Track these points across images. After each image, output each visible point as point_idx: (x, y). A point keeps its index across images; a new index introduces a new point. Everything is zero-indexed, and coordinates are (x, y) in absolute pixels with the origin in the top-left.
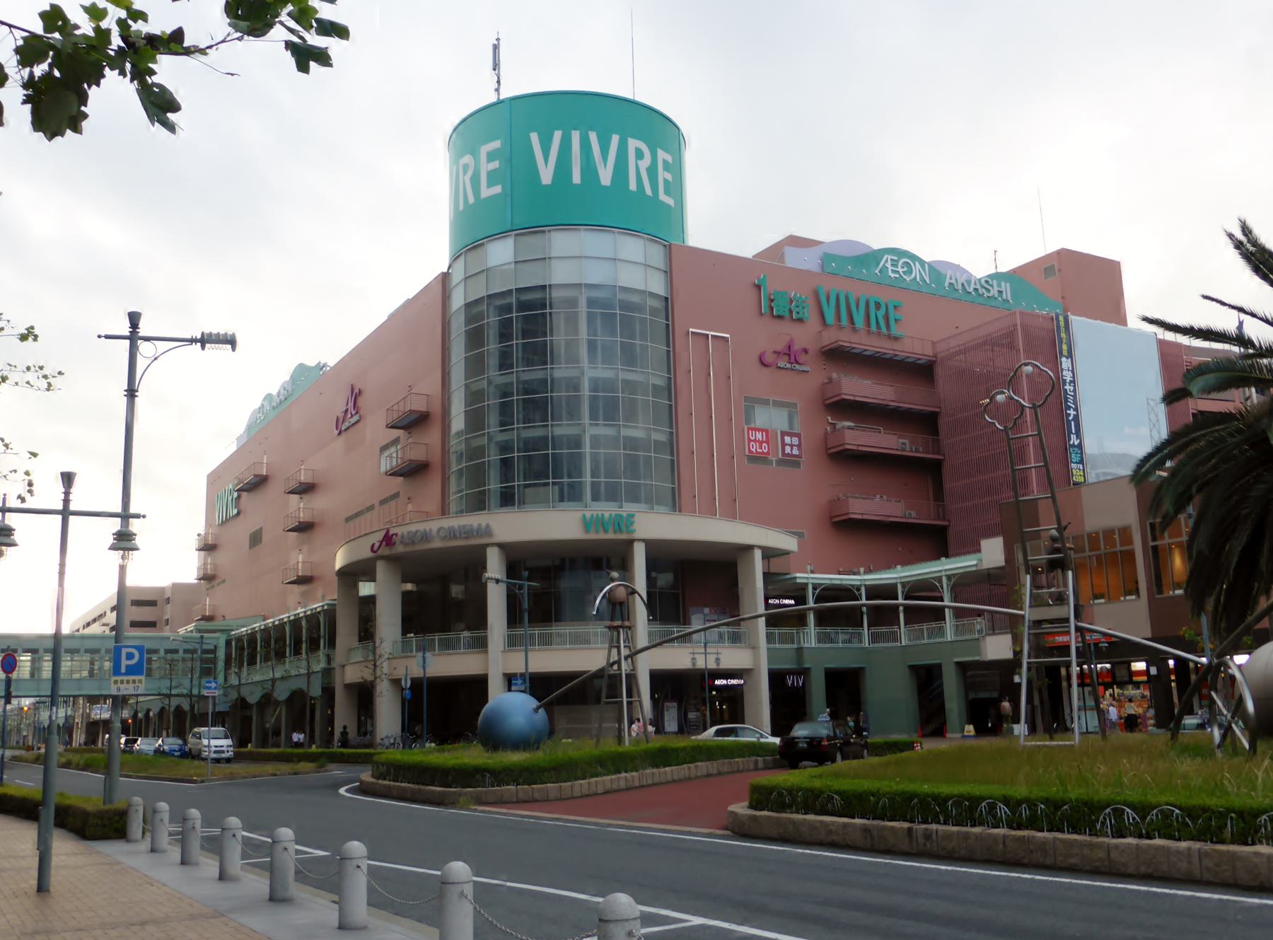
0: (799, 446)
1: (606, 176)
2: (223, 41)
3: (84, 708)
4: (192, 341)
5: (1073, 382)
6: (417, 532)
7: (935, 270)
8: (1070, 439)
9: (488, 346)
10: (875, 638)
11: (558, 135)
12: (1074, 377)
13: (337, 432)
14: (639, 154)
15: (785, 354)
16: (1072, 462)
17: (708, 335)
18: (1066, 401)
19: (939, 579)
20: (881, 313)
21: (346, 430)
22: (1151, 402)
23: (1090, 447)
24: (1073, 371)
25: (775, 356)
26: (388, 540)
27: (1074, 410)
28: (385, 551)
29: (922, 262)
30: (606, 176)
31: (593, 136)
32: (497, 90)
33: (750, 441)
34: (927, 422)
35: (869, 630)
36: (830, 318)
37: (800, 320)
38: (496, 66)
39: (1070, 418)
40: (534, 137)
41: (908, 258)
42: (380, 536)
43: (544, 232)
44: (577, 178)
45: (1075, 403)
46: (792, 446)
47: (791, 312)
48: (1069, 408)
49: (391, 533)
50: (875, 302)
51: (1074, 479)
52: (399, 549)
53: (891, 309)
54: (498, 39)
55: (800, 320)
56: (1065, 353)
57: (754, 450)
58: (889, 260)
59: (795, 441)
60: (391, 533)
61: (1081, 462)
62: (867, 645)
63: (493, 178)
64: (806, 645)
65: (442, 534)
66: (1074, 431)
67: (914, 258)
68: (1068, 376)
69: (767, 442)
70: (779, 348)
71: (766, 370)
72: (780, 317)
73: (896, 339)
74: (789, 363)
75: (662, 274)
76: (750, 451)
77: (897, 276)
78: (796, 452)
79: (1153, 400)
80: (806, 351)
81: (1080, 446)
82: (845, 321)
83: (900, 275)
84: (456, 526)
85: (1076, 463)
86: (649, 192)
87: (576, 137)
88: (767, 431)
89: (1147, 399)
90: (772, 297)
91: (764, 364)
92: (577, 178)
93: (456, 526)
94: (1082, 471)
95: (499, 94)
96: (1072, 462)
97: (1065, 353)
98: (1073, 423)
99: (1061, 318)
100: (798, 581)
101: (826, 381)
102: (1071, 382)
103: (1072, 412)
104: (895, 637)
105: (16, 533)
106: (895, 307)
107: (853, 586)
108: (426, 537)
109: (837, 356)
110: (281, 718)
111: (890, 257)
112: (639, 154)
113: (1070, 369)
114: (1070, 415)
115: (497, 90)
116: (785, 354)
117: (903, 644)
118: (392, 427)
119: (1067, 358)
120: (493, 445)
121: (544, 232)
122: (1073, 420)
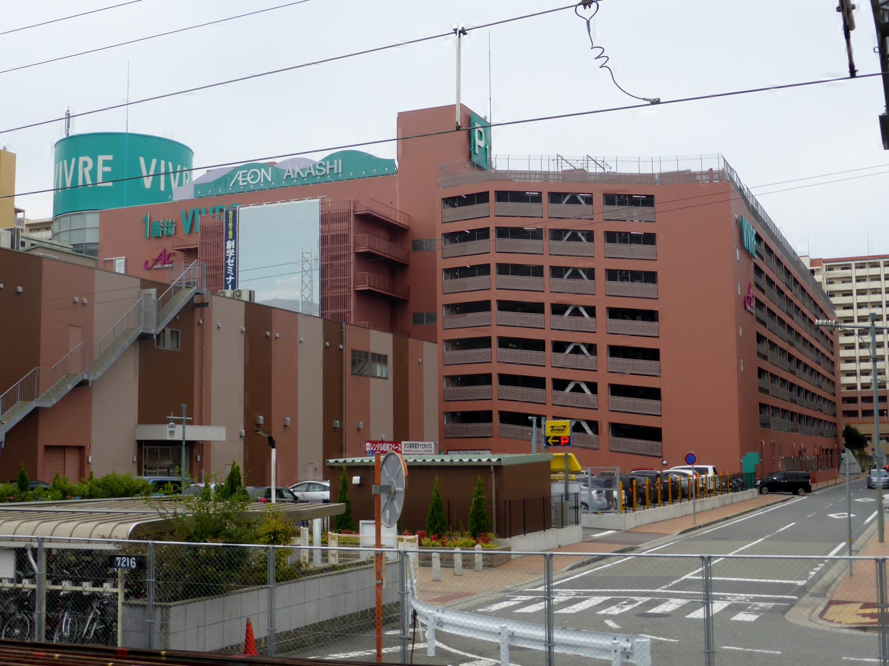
5: (235, 256)
12: (235, 253)
17: (330, 169)
18: (227, 270)
24: (235, 249)
39: (228, 283)
40: (142, 159)
41: (253, 168)
43: (83, 213)
45: (234, 271)
56: (230, 237)
58: (241, 175)
68: (230, 253)
89: (303, 253)
97: (230, 237)
99: (231, 213)
102: (232, 256)
105: (881, 114)
110: (697, 573)
111: (241, 172)
112: (85, 164)
113: (233, 247)
119: (231, 240)
121: (83, 213)
122: (230, 284)
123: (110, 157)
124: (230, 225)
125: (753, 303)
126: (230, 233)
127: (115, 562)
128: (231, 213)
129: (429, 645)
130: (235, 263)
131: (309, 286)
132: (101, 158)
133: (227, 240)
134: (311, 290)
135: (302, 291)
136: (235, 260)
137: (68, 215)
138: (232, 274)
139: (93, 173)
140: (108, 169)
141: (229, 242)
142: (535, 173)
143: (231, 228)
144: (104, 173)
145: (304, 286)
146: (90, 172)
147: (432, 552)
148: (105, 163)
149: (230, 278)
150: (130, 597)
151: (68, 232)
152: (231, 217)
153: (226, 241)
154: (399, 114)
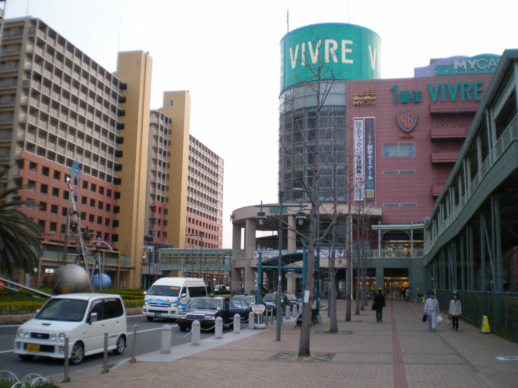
2: (337, 74)
14: (331, 46)
20: (468, 90)
27: (372, 165)
31: (310, 44)
35: (381, 250)
39: (369, 169)
50: (59, 179)
55: (417, 102)
62: (380, 257)
66: (370, 174)
94: (373, 193)
98: (370, 171)
102: (371, 154)
112: (331, 46)
114: (369, 168)
119: (370, 144)
122: (370, 170)
123: (351, 42)
127: (358, 285)
129: (206, 319)
132: (344, 42)
138: (371, 164)
140: (349, 51)
147: (206, 299)
148: (348, 46)
149: (370, 167)
150: (435, 323)
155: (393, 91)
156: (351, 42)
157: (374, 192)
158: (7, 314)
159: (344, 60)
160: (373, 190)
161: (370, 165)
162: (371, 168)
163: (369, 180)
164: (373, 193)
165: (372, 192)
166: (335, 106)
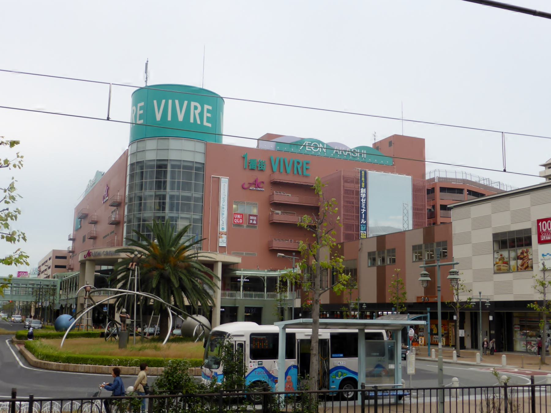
0: (257, 221)
1: (181, 118)
3: (353, 303)
4: (108, 116)
5: (366, 198)
6: (97, 252)
7: (329, 148)
8: (361, 221)
9: (135, 181)
10: (245, 296)
11: (164, 101)
13: (103, 202)
14: (196, 108)
15: (253, 184)
16: (361, 230)
18: (361, 205)
19: (264, 278)
20: (299, 166)
21: (105, 202)
22: (404, 205)
23: (371, 223)
25: (249, 185)
26: (89, 254)
27: (365, 209)
28: (88, 258)
29: (323, 144)
30: (181, 118)
31: (177, 102)
32: (146, 81)
33: (234, 218)
34: (314, 210)
36: (275, 168)
37: (262, 170)
38: (146, 72)
39: (362, 213)
40: (155, 102)
42: (86, 253)
44: (169, 119)
45: (366, 206)
46: (253, 220)
47: (258, 167)
48: (362, 209)
49: (90, 251)
51: (361, 237)
52: (92, 258)
53: (305, 165)
54: (148, 61)
55: (262, 170)
56: (363, 186)
57: (236, 222)
59: (255, 218)
60: (90, 251)
61: (366, 230)
62: (241, 298)
63: (141, 117)
64: (238, 298)
65: (105, 253)
67: (319, 142)
68: (363, 196)
69: (242, 219)
70: (251, 181)
71: (244, 191)
72: (252, 169)
73: (307, 177)
74: (255, 187)
75: (203, 154)
76: (234, 222)
77: (310, 150)
78: (255, 222)
79: (406, 204)
80: (263, 182)
81: (366, 224)
82: (282, 170)
83: (312, 149)
84: (109, 251)
85: (363, 230)
86: (199, 122)
87: (170, 102)
88: (242, 215)
89: (403, 204)
90: (249, 162)
91: (243, 188)
92: (169, 119)
93: (109, 251)
95: (146, 83)
96: (361, 230)
97: (363, 186)
98: (363, 215)
99: (363, 172)
100: (237, 274)
101: (271, 194)
102: (364, 198)
103: (364, 210)
104: (262, 296)
106: (307, 164)
107: (261, 276)
108: (99, 254)
109: (276, 184)
111: (307, 142)
112: (196, 108)
113: (365, 193)
114: (362, 211)
115: (146, 81)
116: (253, 184)
117: (265, 299)
118: (111, 206)
119: (364, 188)
120: (135, 219)
121: (169, 139)
122: (363, 213)
124: (363, 179)
125: (108, 280)
126: (363, 184)
128: (363, 172)
130: (366, 202)
131: (407, 222)
132: (206, 107)
133: (361, 187)
134: (408, 225)
135: (403, 224)
136: (366, 200)
137: (156, 139)
139: (201, 114)
140: (209, 115)
141: (362, 189)
142: (459, 179)
143: (363, 181)
144: (207, 117)
145: (404, 222)
146: (199, 114)
148: (208, 111)
149: (364, 210)
151: (156, 151)
152: (363, 174)
153: (361, 188)
154: (424, 139)
155: (244, 158)
156: (210, 108)
157: (361, 236)
158: (60, 363)
159: (205, 124)
160: (365, 232)
161: (363, 208)
162: (364, 211)
163: (363, 224)
164: (365, 235)
165: (365, 233)
166: (196, 163)
